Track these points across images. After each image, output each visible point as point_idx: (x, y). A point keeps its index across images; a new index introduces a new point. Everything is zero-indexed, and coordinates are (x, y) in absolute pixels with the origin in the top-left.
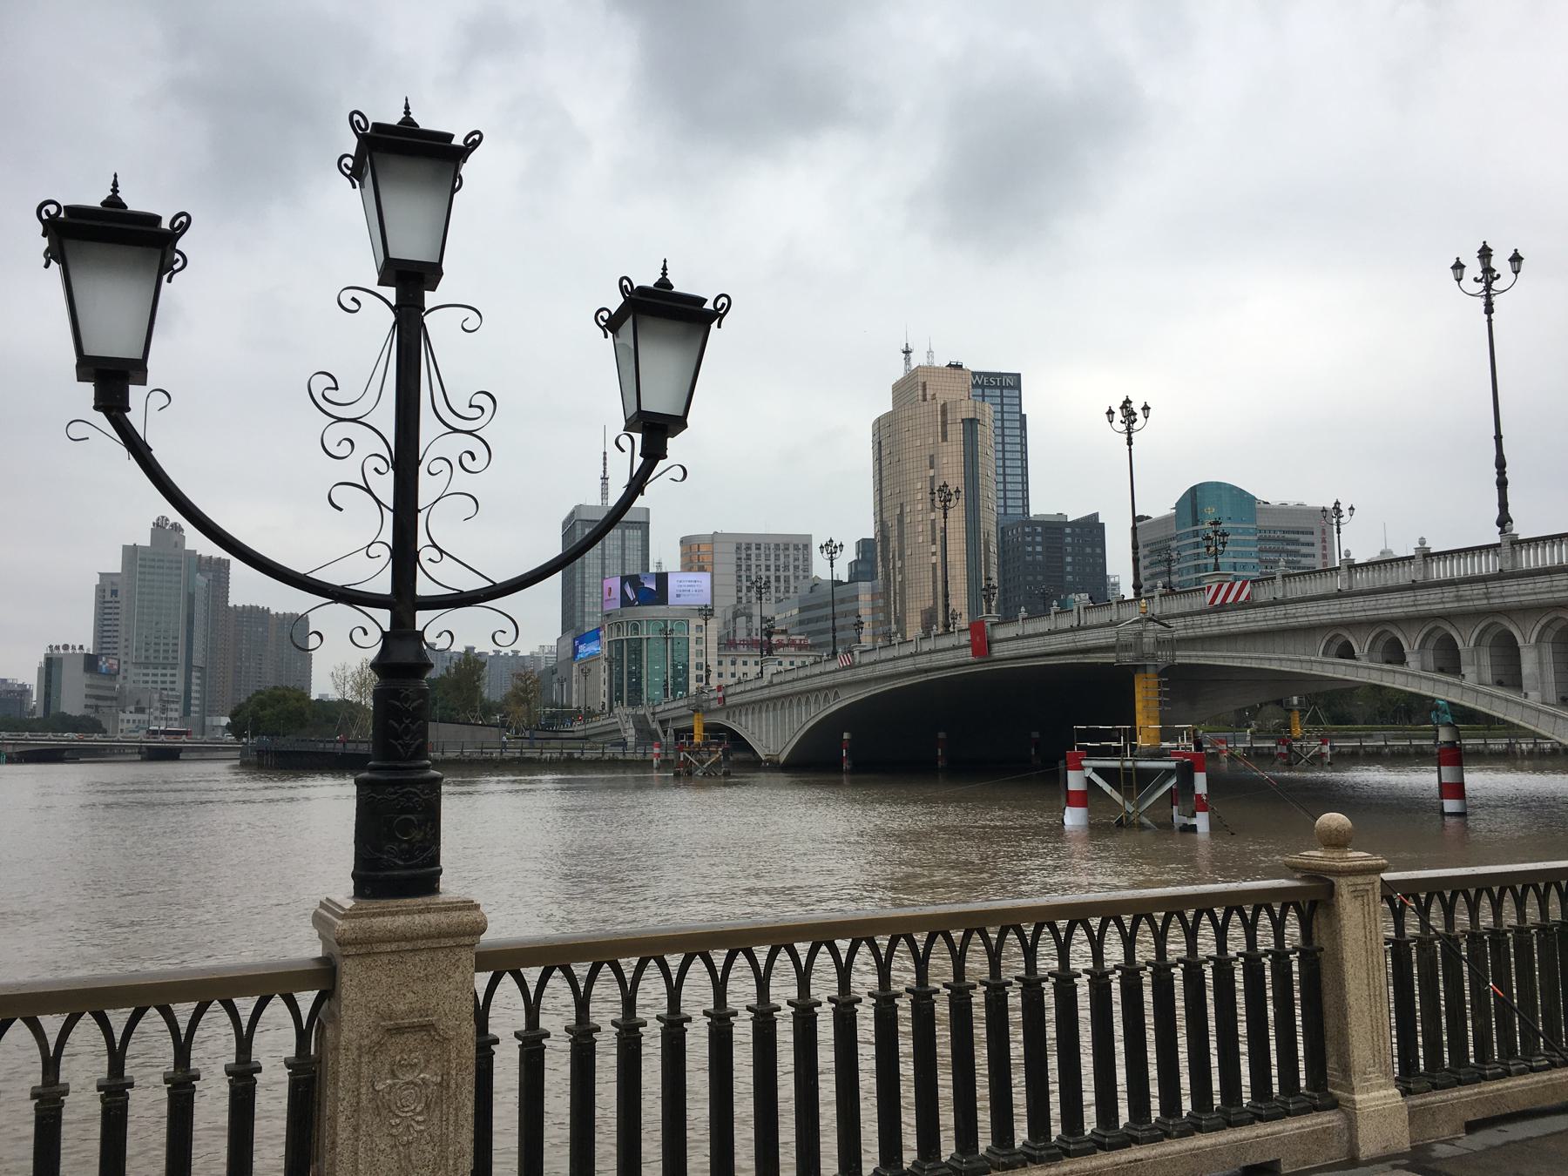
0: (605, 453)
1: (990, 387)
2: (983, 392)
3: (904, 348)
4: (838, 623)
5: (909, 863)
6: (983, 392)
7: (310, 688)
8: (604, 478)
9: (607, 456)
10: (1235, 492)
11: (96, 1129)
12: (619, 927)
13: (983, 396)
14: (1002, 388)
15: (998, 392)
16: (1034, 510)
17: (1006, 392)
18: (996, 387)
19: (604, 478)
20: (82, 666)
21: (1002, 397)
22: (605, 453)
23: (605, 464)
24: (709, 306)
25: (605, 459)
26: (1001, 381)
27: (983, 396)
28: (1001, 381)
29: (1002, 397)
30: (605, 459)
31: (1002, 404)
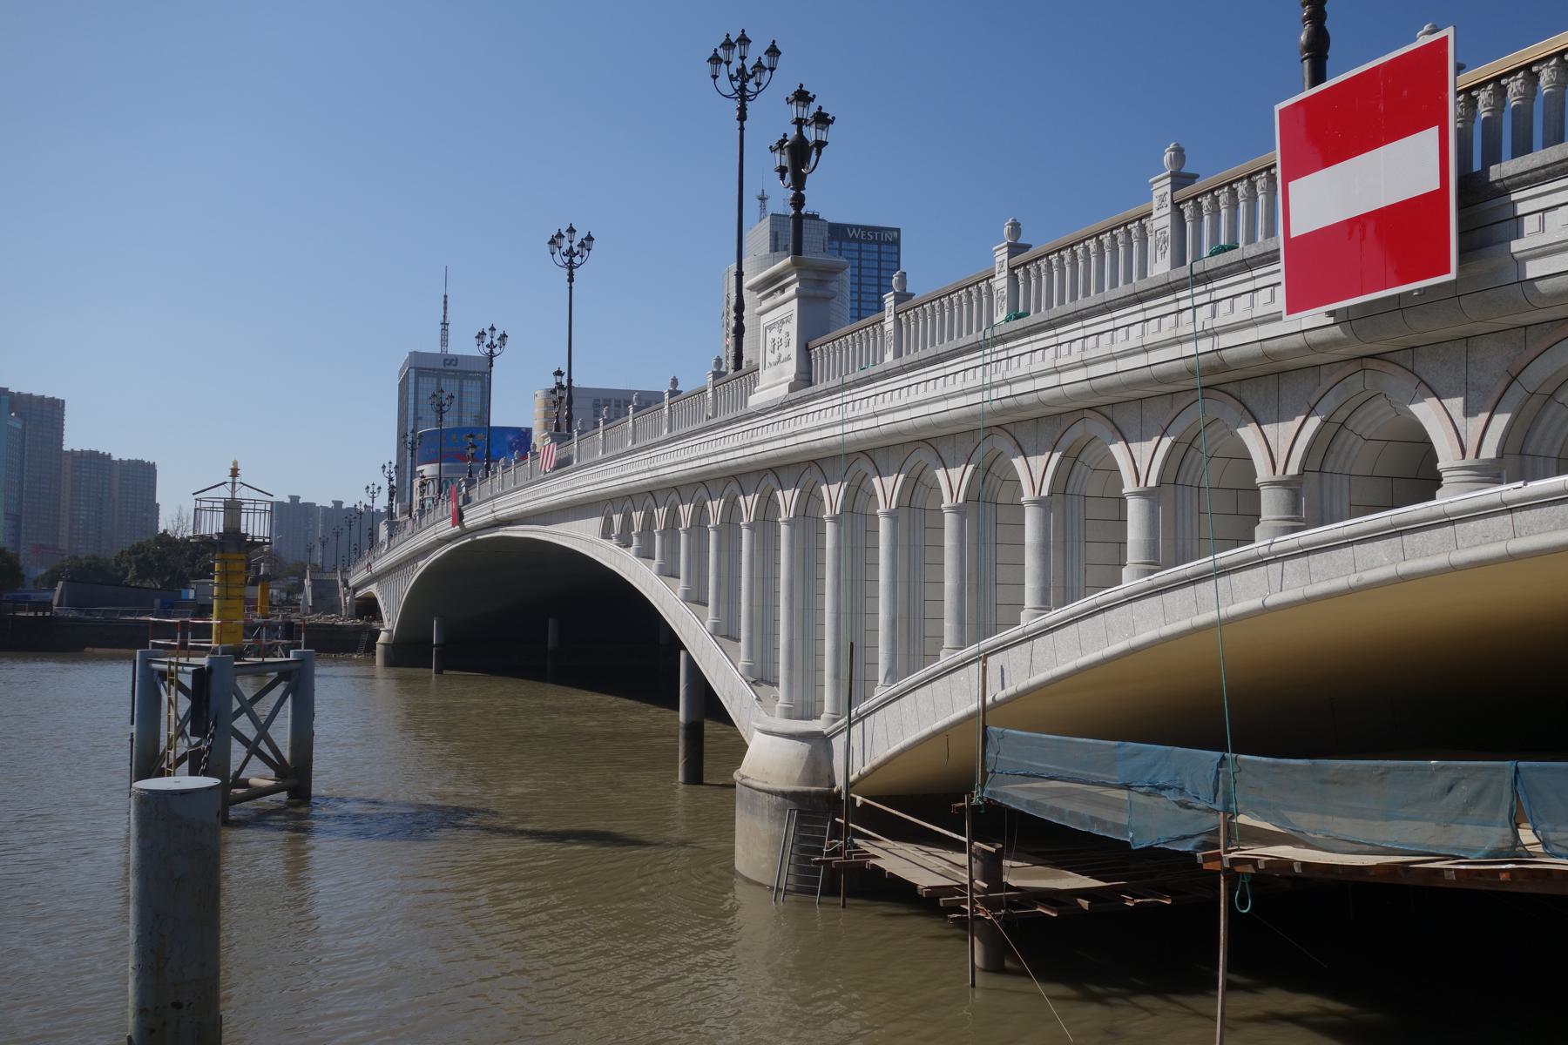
0: (446, 297)
1: (867, 242)
2: (860, 247)
3: (760, 193)
4: (995, 478)
5: (668, 820)
6: (860, 247)
7: (1417, 418)
8: (445, 324)
9: (449, 300)
10: (510, 438)
11: (1409, 822)
12: (387, 845)
13: (840, 250)
14: (879, 243)
15: (875, 247)
16: (496, 421)
17: (884, 248)
18: (873, 241)
19: (445, 324)
20: (158, 468)
21: (880, 252)
22: (446, 297)
23: (445, 308)
24: (830, 117)
25: (445, 302)
26: (879, 235)
27: (840, 250)
28: (879, 235)
29: (880, 252)
30: (445, 302)
31: (860, 259)
